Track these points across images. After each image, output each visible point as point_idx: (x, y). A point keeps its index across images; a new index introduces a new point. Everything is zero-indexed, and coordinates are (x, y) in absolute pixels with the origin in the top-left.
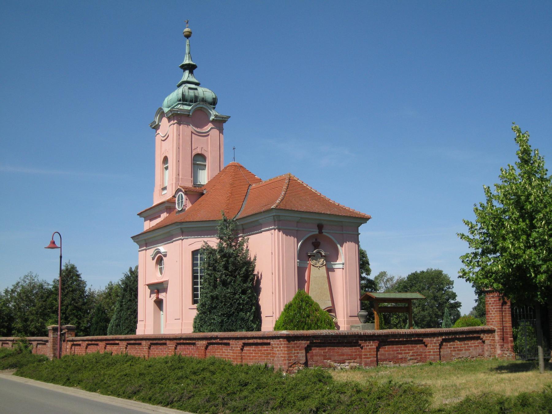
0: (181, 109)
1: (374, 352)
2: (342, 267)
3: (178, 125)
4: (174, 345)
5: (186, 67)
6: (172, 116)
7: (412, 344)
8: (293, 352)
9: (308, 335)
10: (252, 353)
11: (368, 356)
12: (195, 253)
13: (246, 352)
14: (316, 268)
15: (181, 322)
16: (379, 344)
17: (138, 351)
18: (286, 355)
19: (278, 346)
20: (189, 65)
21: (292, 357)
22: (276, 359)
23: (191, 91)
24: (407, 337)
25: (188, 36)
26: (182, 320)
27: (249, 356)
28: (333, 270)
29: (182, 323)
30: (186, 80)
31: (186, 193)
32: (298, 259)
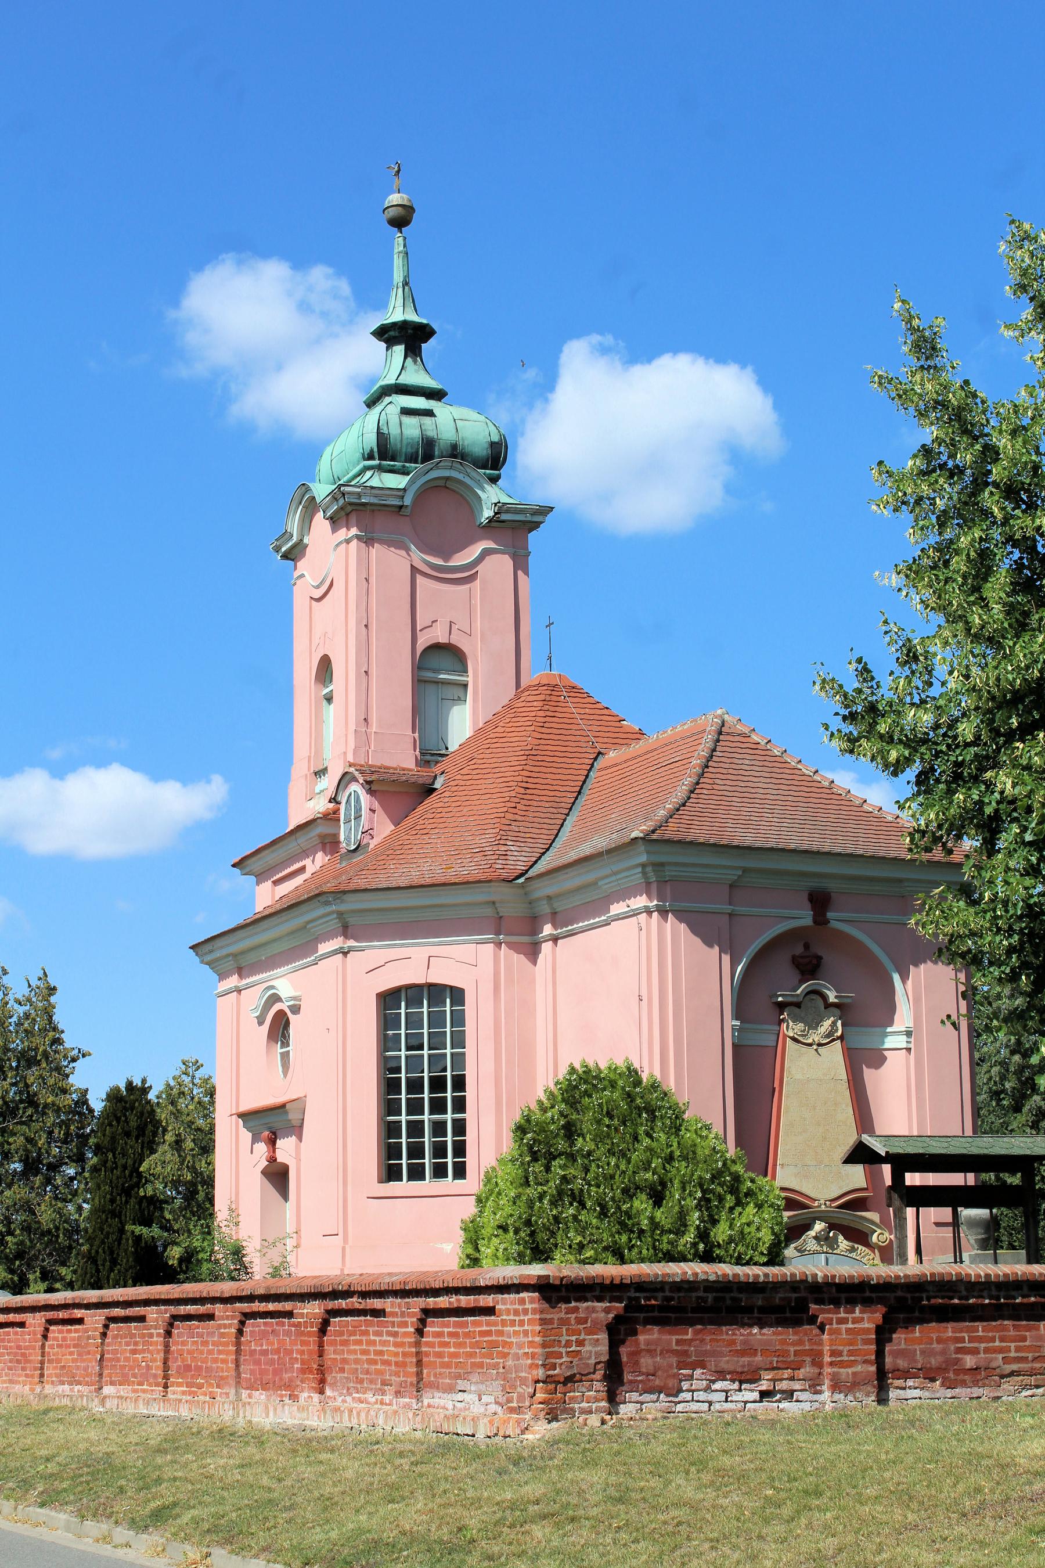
0: (372, 488)
1: (866, 1342)
2: (904, 1045)
3: (364, 545)
4: (236, 1321)
5: (392, 333)
6: (343, 513)
7: (1019, 1319)
8: (564, 1338)
9: (617, 1281)
10: (447, 1344)
11: (846, 1358)
12: (388, 999)
13: (431, 1339)
14: (805, 1048)
15: (342, 1244)
16: (885, 1317)
17: (136, 1344)
18: (539, 1350)
19: (517, 1318)
20: (404, 325)
21: (560, 1356)
22: (510, 1363)
23: (410, 421)
24: (964, 1293)
25: (401, 221)
26: (345, 1240)
27: (439, 1355)
28: (878, 1059)
29: (344, 1249)
30: (393, 382)
31: (370, 786)
32: (737, 1015)
